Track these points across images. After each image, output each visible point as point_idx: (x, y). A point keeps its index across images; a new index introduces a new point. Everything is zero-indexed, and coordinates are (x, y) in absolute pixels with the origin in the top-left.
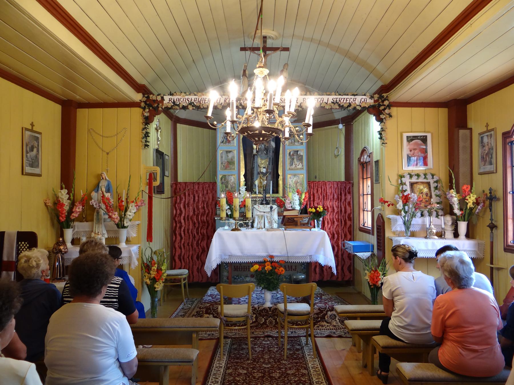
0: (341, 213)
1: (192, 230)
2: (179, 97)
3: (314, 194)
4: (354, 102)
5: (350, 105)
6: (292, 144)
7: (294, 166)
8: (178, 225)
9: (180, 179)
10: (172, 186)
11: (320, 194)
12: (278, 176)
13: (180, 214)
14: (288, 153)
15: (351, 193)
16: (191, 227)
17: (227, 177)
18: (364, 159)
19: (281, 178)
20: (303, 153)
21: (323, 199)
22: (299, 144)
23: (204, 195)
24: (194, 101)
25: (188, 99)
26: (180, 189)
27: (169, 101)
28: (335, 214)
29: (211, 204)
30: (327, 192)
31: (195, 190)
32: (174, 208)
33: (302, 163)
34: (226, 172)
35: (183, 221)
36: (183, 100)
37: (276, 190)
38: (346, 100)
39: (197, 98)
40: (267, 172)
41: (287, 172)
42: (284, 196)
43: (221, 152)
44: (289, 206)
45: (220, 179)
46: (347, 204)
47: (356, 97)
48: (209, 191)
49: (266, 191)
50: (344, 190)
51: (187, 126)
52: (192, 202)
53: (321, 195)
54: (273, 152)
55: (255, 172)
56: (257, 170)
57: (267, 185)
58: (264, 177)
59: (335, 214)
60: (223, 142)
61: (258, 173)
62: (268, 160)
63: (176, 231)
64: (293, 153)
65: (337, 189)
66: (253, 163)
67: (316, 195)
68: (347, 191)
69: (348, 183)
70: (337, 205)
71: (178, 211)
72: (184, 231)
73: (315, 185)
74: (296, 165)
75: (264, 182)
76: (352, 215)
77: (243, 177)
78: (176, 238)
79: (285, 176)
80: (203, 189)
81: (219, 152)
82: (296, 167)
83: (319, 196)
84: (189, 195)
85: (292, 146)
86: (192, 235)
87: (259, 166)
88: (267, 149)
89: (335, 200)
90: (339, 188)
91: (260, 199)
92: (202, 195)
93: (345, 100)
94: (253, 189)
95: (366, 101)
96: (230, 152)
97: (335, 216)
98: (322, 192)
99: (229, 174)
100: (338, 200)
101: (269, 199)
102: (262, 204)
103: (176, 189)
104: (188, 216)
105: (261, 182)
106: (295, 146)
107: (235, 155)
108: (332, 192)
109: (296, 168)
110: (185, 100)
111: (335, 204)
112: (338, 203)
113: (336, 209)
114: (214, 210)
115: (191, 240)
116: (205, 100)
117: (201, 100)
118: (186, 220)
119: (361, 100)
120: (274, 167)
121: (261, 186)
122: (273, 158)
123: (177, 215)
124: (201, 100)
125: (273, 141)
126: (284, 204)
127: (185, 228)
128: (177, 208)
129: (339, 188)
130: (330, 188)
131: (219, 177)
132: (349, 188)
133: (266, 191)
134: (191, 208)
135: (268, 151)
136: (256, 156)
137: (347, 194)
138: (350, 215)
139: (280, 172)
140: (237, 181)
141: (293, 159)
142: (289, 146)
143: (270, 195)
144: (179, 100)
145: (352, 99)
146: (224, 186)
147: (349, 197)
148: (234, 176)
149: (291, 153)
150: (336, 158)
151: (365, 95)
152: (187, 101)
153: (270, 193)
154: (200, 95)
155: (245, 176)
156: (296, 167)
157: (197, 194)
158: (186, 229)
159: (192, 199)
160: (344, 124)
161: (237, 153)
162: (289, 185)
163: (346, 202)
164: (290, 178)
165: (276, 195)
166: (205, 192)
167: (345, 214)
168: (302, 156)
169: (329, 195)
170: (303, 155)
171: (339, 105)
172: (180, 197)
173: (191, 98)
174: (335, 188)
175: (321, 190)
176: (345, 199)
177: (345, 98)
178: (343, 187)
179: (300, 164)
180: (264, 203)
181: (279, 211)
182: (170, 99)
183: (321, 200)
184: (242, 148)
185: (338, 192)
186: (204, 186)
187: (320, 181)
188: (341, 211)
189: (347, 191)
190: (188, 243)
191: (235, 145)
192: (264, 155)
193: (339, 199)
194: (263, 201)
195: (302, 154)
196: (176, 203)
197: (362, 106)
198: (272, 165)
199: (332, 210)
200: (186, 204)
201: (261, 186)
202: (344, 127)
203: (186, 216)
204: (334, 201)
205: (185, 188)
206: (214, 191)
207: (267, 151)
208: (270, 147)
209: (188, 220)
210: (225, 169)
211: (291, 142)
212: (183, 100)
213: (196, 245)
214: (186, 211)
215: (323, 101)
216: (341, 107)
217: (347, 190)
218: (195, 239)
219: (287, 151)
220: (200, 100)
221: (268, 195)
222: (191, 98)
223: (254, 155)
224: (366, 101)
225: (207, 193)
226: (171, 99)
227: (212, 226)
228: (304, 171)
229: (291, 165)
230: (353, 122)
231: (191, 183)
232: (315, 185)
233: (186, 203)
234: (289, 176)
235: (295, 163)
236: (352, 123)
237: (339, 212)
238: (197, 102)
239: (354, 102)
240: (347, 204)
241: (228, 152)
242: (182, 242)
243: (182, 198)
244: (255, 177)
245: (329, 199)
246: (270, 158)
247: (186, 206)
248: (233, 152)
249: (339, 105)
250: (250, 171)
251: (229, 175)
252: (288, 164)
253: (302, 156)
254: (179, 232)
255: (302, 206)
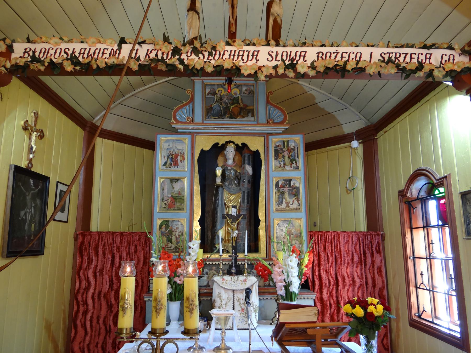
0: (367, 287)
1: (105, 318)
2: (47, 46)
3: (319, 253)
4: (427, 62)
5: (420, 66)
6: (280, 169)
7: (284, 205)
8: (82, 308)
9: (95, 227)
10: (76, 239)
11: (329, 253)
12: (257, 221)
13: (87, 289)
14: (274, 183)
15: (382, 251)
16: (103, 313)
17: (170, 223)
18: (411, 192)
19: (262, 225)
20: (299, 183)
21: (334, 263)
22: (292, 169)
23: (129, 253)
24: (80, 54)
25: (67, 50)
26: (89, 243)
27: (24, 53)
28: (356, 289)
29: (141, 271)
30: (340, 251)
31: (115, 245)
32: (77, 277)
33: (298, 200)
34: (169, 215)
35: (90, 302)
36: (56, 53)
37: (254, 248)
38: (411, 58)
39: (85, 49)
40: (238, 216)
41: (273, 215)
42: (269, 257)
43: (162, 180)
44: (279, 278)
45: (158, 227)
46: (376, 271)
47: (431, 51)
48: (139, 248)
49: (237, 249)
50: (370, 246)
51: (115, 142)
52: (109, 266)
53: (332, 255)
54: (249, 181)
55: (219, 215)
56: (222, 210)
57: (240, 238)
58: (233, 223)
59: (356, 289)
60: (165, 164)
61: (224, 217)
62: (241, 195)
63: (77, 320)
64: (282, 183)
65: (358, 245)
66: (215, 200)
67: (322, 255)
68: (374, 249)
69: (375, 235)
70: (359, 274)
71: (84, 283)
72: (91, 320)
73: (321, 238)
74: (288, 203)
75: (233, 232)
76: (385, 292)
77: (198, 223)
78: (76, 333)
79: (269, 222)
80: (130, 244)
81: (159, 181)
82: (288, 206)
83: (328, 257)
84: (104, 253)
85: (281, 172)
86: (106, 328)
87: (225, 204)
88: (238, 178)
89: (355, 265)
90: (361, 243)
91: (227, 263)
92: (127, 256)
93: (408, 57)
94: (215, 244)
95: (454, 59)
96: (177, 180)
97: (358, 293)
98: (332, 250)
99: (175, 218)
100: (361, 265)
101: (243, 263)
102: (230, 274)
103: (82, 243)
104: (100, 293)
105: (228, 233)
106: (287, 172)
107: (186, 187)
108: (350, 250)
109: (288, 208)
110: (60, 53)
111: (357, 272)
112: (361, 269)
113: (357, 280)
114: (145, 281)
115: (102, 337)
116: (103, 54)
117: (94, 53)
118: (96, 300)
119: (442, 58)
120: (250, 207)
121: (228, 240)
122: (248, 193)
123: (82, 291)
124: (94, 53)
125: (249, 164)
126: (270, 273)
127: (93, 313)
128: (83, 277)
129: (361, 243)
130: (346, 243)
131: (157, 223)
132: (378, 243)
133: (237, 249)
134: (106, 277)
135: (242, 180)
136: (220, 189)
137: (376, 255)
138: (383, 292)
139: (261, 215)
140: (186, 230)
141: (283, 193)
142: (276, 173)
143: (245, 255)
144: (47, 51)
145: (424, 56)
146: (165, 239)
147: (378, 259)
148: (183, 222)
149: (280, 184)
150: (348, 194)
151: (450, 48)
152: (63, 53)
153: (244, 251)
154: (93, 43)
155: (201, 221)
156: (288, 206)
157: (119, 252)
158: (95, 316)
159: (110, 262)
160: (360, 141)
161: (189, 183)
162: (277, 237)
163: (373, 267)
164: (279, 225)
165: (253, 256)
166: (133, 249)
167: (373, 289)
168: (298, 188)
169: (346, 255)
170: (299, 187)
171: (398, 66)
172: (89, 258)
173: (74, 49)
174: (354, 243)
175: (332, 246)
176: (373, 263)
177: (407, 54)
178: (368, 242)
179: (296, 201)
180: (234, 271)
181: (260, 284)
182: (26, 49)
183: (332, 264)
184: (196, 174)
185: (360, 250)
186: (132, 239)
187: (328, 232)
188: (367, 283)
189: (374, 249)
190: (97, 343)
191: (186, 170)
192: (234, 186)
193: (362, 262)
194: (231, 266)
195: (297, 185)
196: (80, 268)
197: (447, 69)
198: (248, 203)
199: (351, 282)
200: (98, 270)
201: (228, 240)
202: (361, 145)
203: (97, 292)
204: (355, 267)
205: (99, 242)
206: (148, 248)
207: (239, 180)
208: (244, 173)
209: (99, 298)
210: (168, 210)
211: (279, 165)
212: (56, 53)
213: (112, 346)
214: (98, 283)
215: (360, 57)
216: (401, 70)
217: (374, 246)
218: (109, 336)
219: (273, 181)
220: (92, 52)
221: (240, 256)
222: (74, 49)
223: (218, 186)
224: (454, 59)
225: (136, 251)
226: (28, 50)
227: (141, 311)
228: (302, 214)
229: (280, 203)
230: (377, 136)
231: (108, 233)
232: (321, 238)
233: (99, 268)
234: (276, 222)
235: (286, 200)
236: (376, 138)
237: (364, 284)
238: (85, 56)
239: (427, 62)
240: (376, 271)
241: (174, 181)
242: (87, 342)
243: (92, 259)
244: (218, 223)
245: (345, 262)
246: (244, 192)
247: (98, 274)
248: (182, 182)
249: (398, 66)
250: (211, 213)
251: (173, 221)
252: (274, 202)
253: (298, 188)
254: (83, 321)
255: (303, 277)
